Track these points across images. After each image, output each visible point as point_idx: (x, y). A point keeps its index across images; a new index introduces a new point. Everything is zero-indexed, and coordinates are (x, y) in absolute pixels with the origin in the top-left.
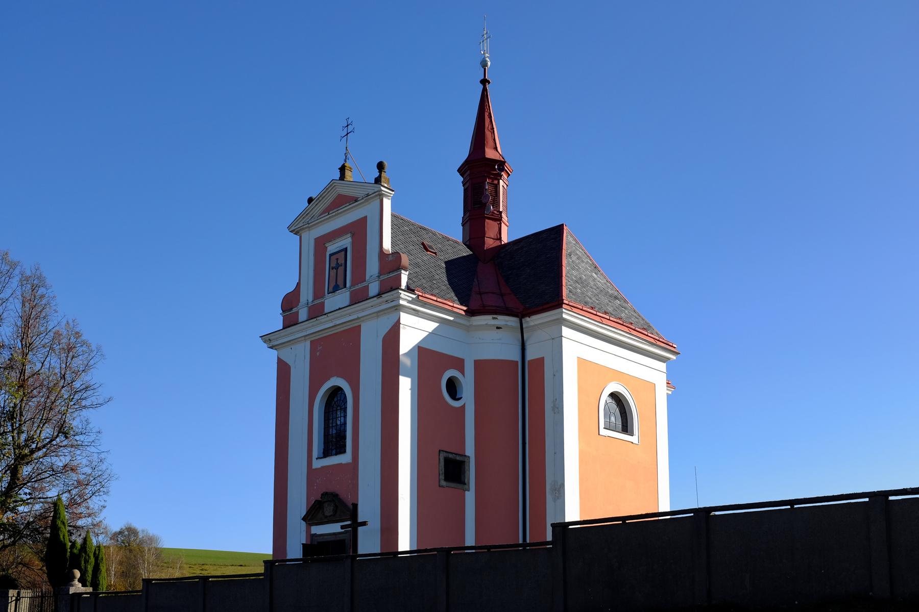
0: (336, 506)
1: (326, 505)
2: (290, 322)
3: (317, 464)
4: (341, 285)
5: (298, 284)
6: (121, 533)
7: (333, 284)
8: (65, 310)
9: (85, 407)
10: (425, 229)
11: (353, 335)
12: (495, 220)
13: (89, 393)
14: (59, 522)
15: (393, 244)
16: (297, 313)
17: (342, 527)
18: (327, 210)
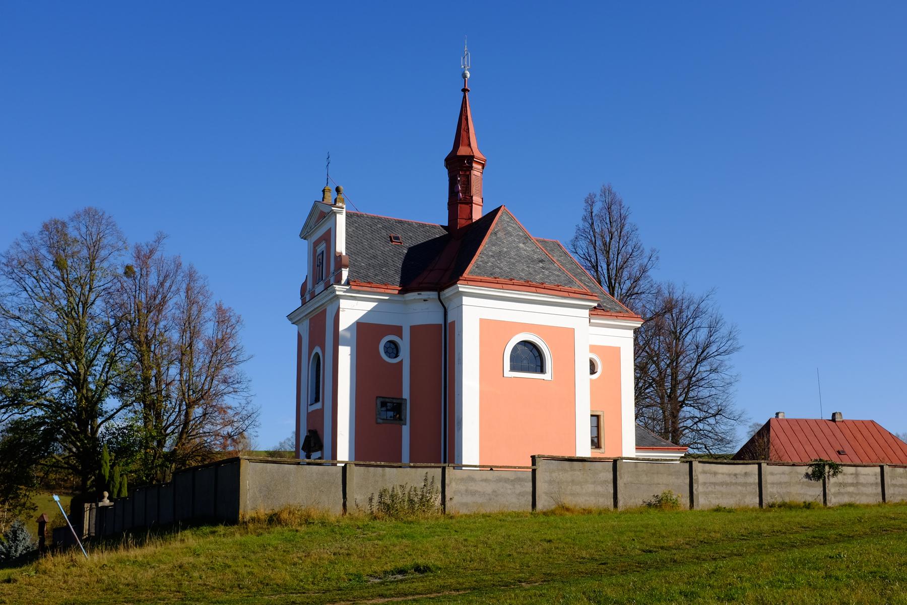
10: (400, 222)
12: (467, 203)
18: (318, 221)
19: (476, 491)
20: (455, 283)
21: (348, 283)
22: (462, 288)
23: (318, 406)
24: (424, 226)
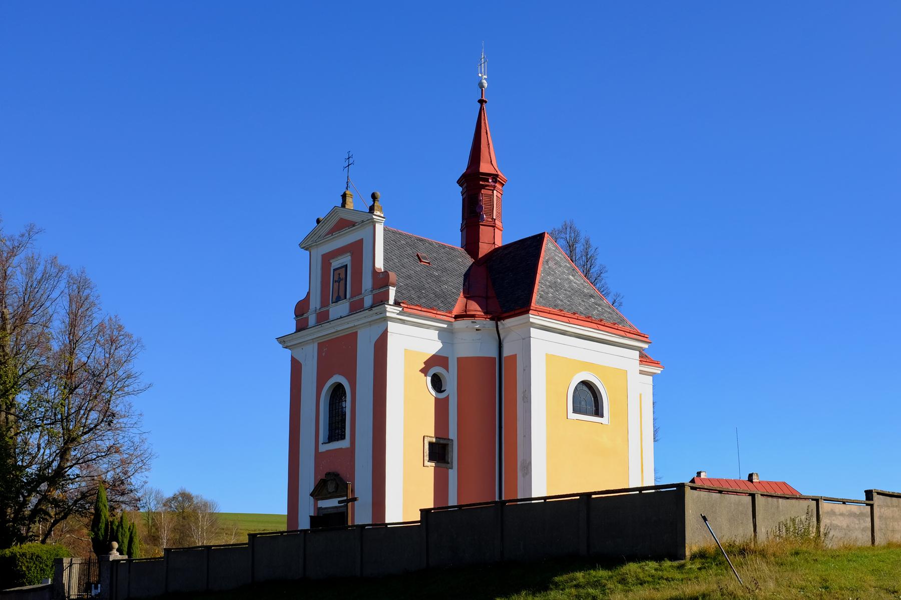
0: (337, 485)
1: (329, 483)
2: (301, 326)
3: (323, 448)
4: (342, 297)
5: (308, 293)
6: (174, 498)
7: (336, 295)
8: (107, 306)
9: (128, 394)
10: (421, 240)
11: (352, 337)
13: (130, 380)
14: (101, 505)
15: (386, 259)
16: (307, 318)
17: (340, 502)
18: (331, 232)
19: (837, 526)
20: (527, 312)
21: (397, 303)
22: (534, 318)
23: (344, 444)
24: (444, 247)
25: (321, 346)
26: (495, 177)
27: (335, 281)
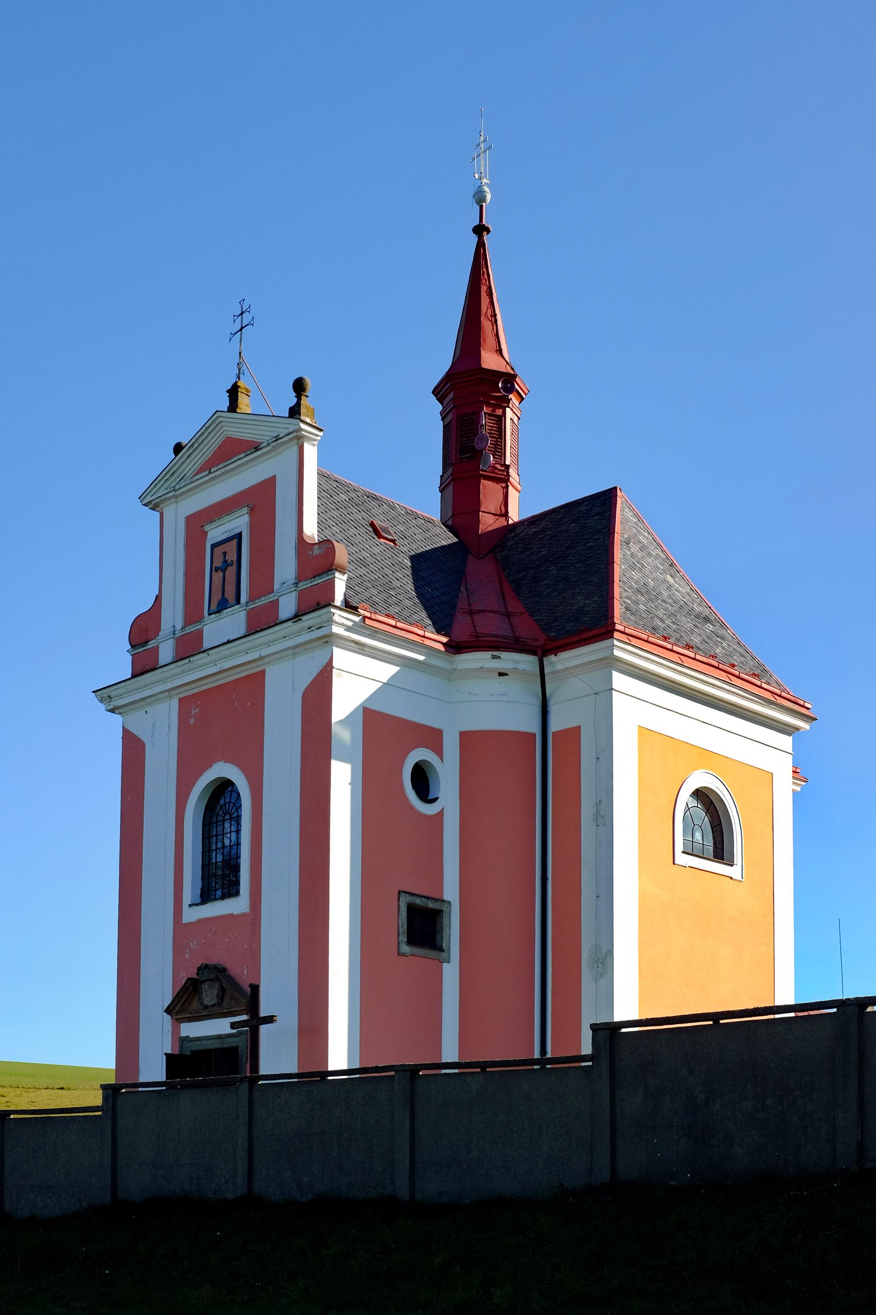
0: (223, 990)
1: (205, 986)
2: (144, 665)
3: (191, 915)
4: (232, 600)
5: (158, 598)
10: (375, 498)
11: (252, 686)
16: (156, 649)
17: (233, 1025)
18: (208, 466)
22: (621, 650)
23: (238, 905)
25: (184, 703)
26: (510, 379)
27: (214, 569)
